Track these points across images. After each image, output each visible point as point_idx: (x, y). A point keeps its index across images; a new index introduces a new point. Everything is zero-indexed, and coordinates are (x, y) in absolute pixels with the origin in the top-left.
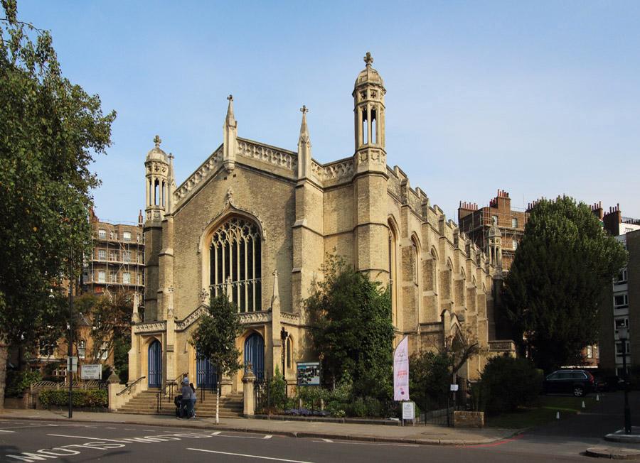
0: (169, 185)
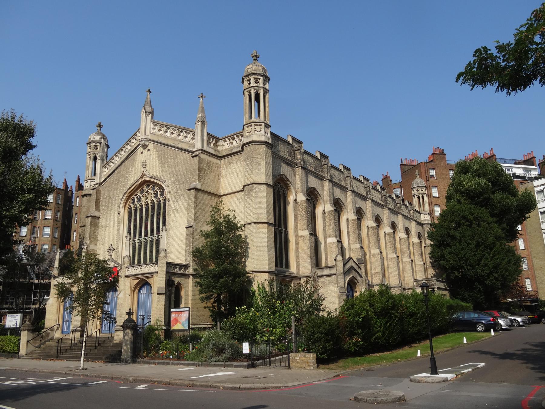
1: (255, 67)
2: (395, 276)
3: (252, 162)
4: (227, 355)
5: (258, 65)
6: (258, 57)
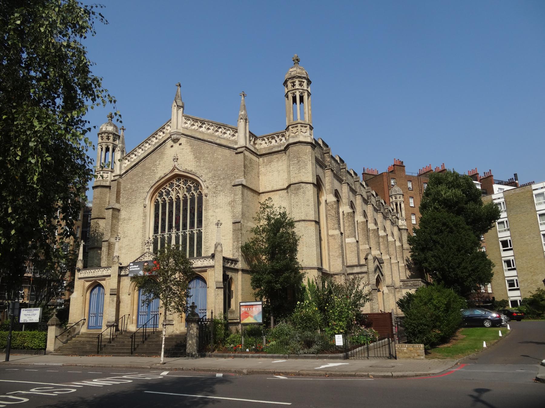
0: (113, 150)
1: (299, 70)
2: (389, 276)
3: (299, 162)
4: (315, 347)
5: (302, 69)
6: (299, 61)
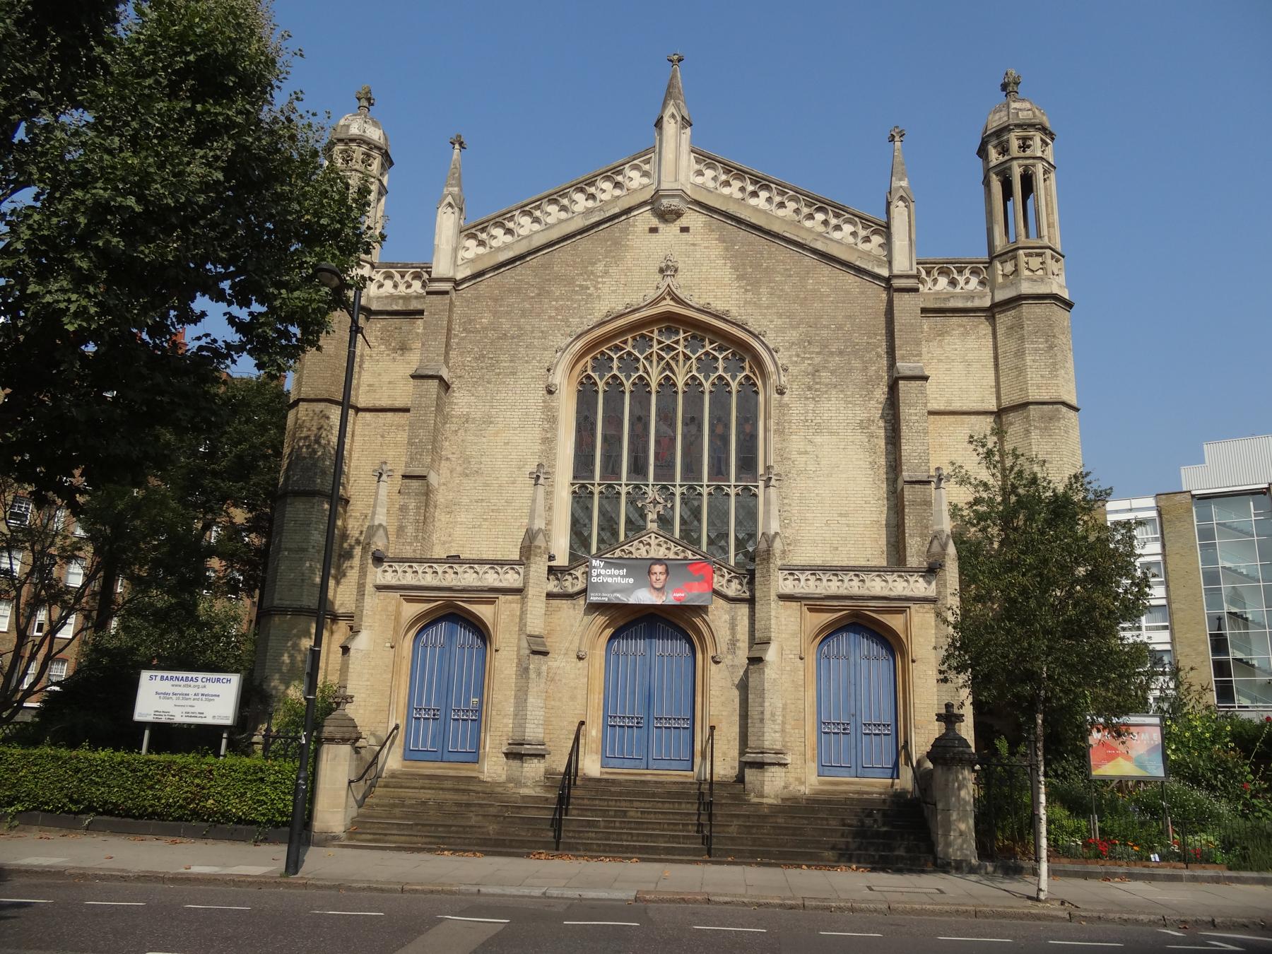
6: (373, 105)
